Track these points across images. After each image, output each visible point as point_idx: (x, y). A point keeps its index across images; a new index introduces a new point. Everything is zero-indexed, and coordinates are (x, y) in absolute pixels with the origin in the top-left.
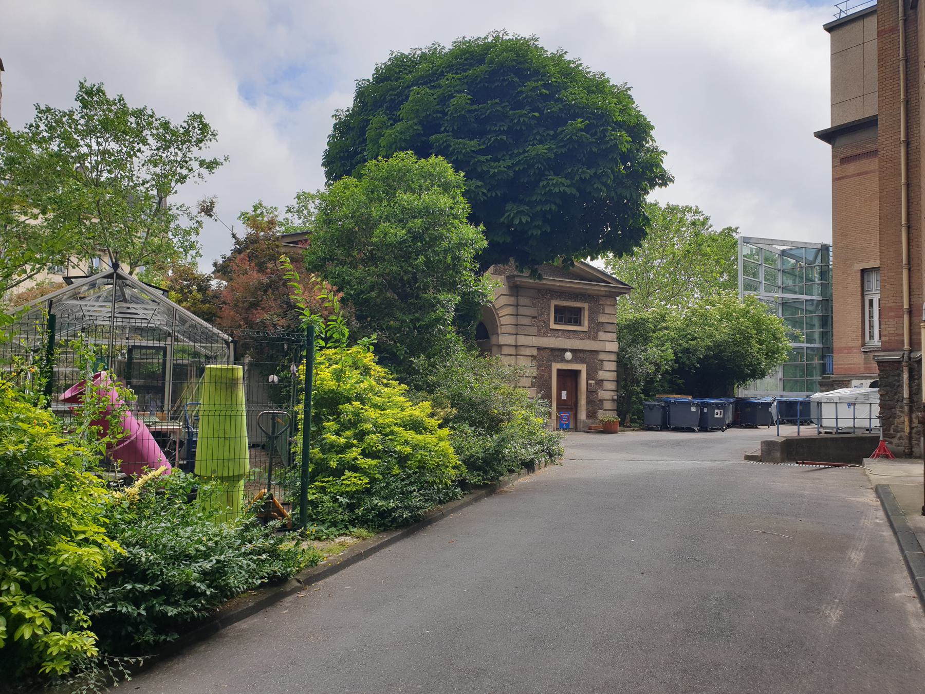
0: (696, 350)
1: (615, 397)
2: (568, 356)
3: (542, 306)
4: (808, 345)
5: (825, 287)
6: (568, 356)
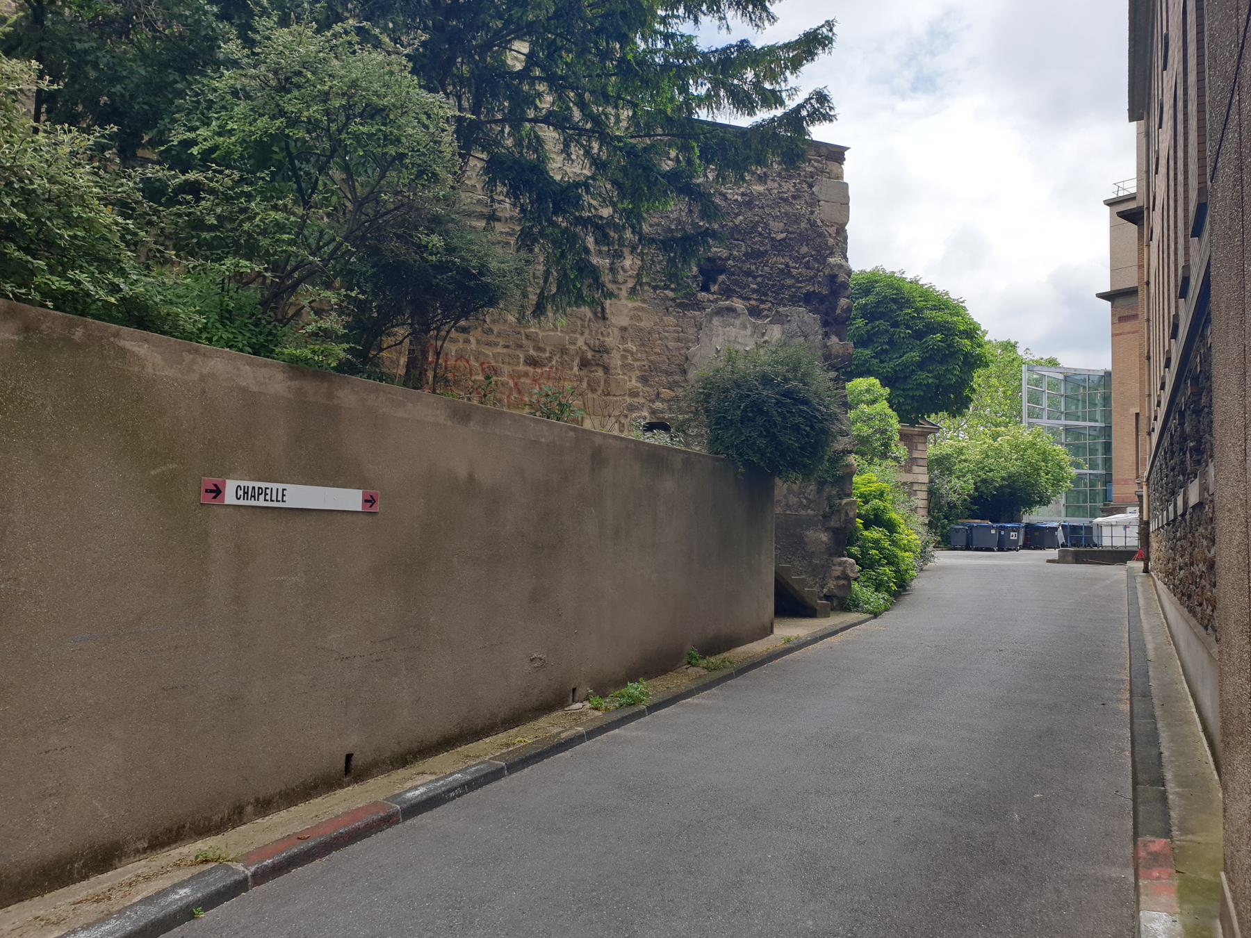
0: (993, 480)
4: (1091, 472)
5: (1107, 415)
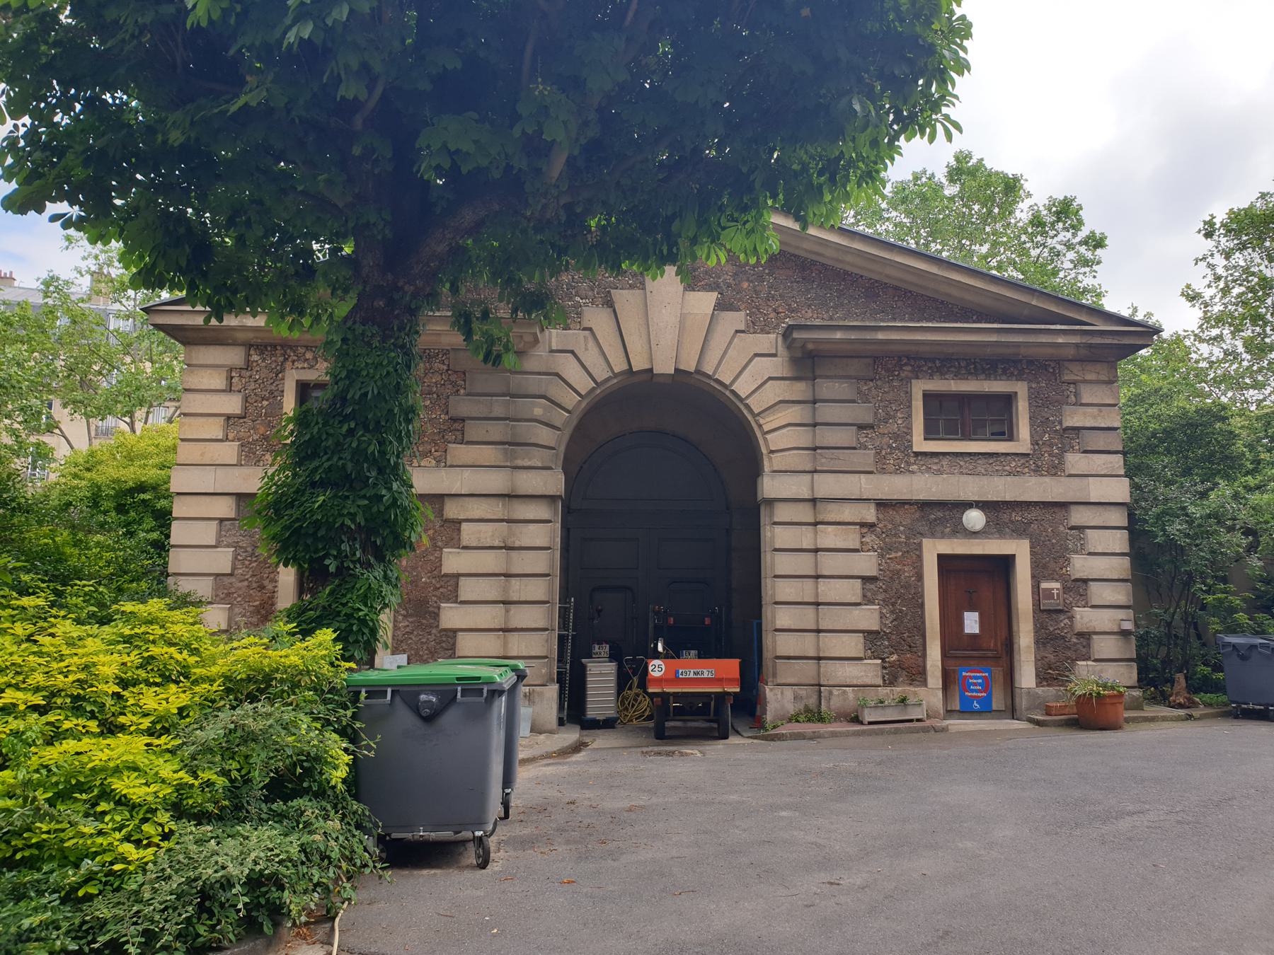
1: (1128, 626)
2: (975, 519)
3: (890, 396)
6: (975, 519)
